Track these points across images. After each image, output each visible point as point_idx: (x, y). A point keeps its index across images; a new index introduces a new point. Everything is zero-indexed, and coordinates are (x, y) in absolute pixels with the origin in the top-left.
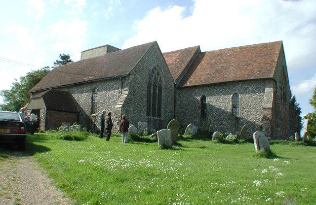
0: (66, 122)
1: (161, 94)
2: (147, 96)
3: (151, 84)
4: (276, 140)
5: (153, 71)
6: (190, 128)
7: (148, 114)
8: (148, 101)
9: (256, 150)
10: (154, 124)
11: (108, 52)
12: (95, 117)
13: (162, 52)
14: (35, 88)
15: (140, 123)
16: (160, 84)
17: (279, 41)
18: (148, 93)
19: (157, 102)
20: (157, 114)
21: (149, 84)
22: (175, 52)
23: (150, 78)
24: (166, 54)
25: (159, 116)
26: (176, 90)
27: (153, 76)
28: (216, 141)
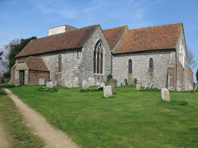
2: (94, 60)
5: (97, 44)
8: (94, 63)
12: (60, 74)
14: (20, 54)
15: (90, 79)
19: (100, 64)
21: (95, 52)
25: (101, 73)
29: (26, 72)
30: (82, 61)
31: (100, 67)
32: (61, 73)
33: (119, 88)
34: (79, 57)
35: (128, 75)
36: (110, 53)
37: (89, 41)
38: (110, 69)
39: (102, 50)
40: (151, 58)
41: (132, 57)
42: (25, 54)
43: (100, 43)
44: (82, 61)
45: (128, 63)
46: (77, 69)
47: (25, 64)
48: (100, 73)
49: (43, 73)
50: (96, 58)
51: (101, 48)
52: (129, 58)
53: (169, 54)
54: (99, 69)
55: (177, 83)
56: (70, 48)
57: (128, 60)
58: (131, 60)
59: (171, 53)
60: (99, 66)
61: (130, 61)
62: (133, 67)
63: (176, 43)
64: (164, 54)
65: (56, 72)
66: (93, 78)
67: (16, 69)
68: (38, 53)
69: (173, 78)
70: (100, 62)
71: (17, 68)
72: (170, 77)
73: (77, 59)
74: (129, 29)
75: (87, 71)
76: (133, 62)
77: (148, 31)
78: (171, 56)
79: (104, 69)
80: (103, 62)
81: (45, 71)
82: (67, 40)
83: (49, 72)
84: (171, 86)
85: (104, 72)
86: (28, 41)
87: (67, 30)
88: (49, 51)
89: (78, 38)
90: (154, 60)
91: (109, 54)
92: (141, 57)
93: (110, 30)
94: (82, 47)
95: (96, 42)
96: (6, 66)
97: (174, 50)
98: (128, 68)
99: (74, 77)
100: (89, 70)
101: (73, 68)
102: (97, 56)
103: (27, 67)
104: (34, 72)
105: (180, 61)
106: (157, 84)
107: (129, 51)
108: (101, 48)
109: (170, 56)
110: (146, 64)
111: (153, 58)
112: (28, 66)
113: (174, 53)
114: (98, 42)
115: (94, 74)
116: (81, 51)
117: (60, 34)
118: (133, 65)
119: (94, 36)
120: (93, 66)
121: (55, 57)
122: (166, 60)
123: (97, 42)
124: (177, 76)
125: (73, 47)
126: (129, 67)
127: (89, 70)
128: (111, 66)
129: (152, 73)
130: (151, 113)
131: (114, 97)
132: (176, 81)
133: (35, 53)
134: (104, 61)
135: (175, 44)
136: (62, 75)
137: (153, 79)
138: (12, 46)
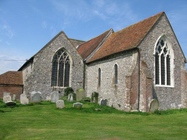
25: (169, 83)
38: (82, 80)
39: (68, 59)
48: (63, 86)
49: (15, 87)
57: (97, 69)
59: (133, 55)
61: (100, 70)
64: (127, 58)
74: (115, 31)
75: (41, 84)
76: (102, 72)
80: (70, 73)
81: (18, 85)
85: (71, 84)
90: (118, 67)
91: (80, 63)
93: (99, 37)
100: (45, 83)
104: (3, 86)
106: (120, 99)
111: (118, 65)
114: (59, 52)
115: (52, 87)
120: (50, 78)
127: (45, 83)
129: (116, 85)
134: (71, 72)
137: (117, 93)
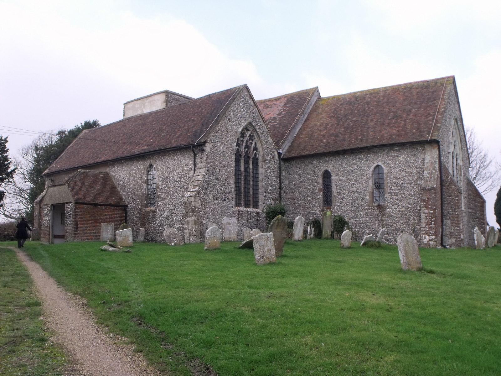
0: (107, 222)
1: (257, 170)
2: (235, 174)
3: (240, 155)
4: (343, 232)
5: (243, 134)
6: (27, 324)
7: (238, 204)
8: (237, 182)
9: (361, 244)
10: (248, 219)
11: (167, 101)
12: (153, 212)
13: (256, 98)
14: (55, 166)
15: (225, 220)
16: (256, 153)
17: (448, 77)
18: (236, 170)
19: (251, 183)
20: (251, 202)
21: (238, 156)
22: (278, 99)
23: (238, 145)
24: (264, 102)
25: (256, 205)
26: (282, 163)
27: (243, 141)
28: (35, 155)
29: (69, 209)
30: (204, 176)
31: (251, 191)
32: (154, 208)
33: (296, 241)
34: (197, 167)
35: (323, 210)
36: (277, 157)
37: (222, 126)
39: (256, 149)
40: (378, 166)
41: (331, 166)
42: (68, 166)
43: (249, 133)
44: (204, 176)
45: (320, 180)
46: (193, 198)
47: (65, 188)
48: (251, 206)
50: (242, 169)
51: (253, 145)
52: (323, 169)
53: (422, 156)
54: (248, 196)
55: (444, 227)
56: (175, 144)
57: (320, 174)
58: (329, 173)
60: (249, 189)
62: (334, 189)
63: (440, 127)
65: (142, 206)
66: (234, 220)
67: (45, 202)
68: (99, 160)
69: (434, 213)
70: (251, 180)
71: (47, 201)
72: (426, 211)
73: (193, 172)
75: (219, 202)
76: (334, 177)
77: (369, 100)
78: (428, 158)
79: (261, 197)
82: (168, 126)
83: (127, 206)
84: (429, 235)
86: (74, 134)
87: (169, 104)
88: (125, 155)
89: (194, 121)
90: (385, 171)
92: (354, 164)
94: (205, 142)
95: (240, 130)
96: (26, 199)
97: (435, 143)
98: (321, 193)
99: (186, 217)
101: (183, 196)
102: (242, 164)
103: (70, 195)
105: (451, 171)
106: (394, 230)
107: (323, 150)
108: (253, 145)
109: (423, 160)
110: (367, 181)
111: (383, 166)
112: (74, 192)
113: (435, 152)
114: (246, 129)
116: (203, 151)
117: (151, 113)
118: (333, 185)
119: (235, 116)
120: (233, 190)
121: (139, 167)
122: (415, 171)
123: (243, 130)
124: (444, 208)
125: (183, 143)
126: (324, 189)
127: (225, 200)
128: (280, 188)
130: (479, 295)
131: (279, 264)
132: (442, 221)
133: (91, 162)
135: (436, 129)
136: (159, 213)
137: (386, 218)
138: (37, 149)
